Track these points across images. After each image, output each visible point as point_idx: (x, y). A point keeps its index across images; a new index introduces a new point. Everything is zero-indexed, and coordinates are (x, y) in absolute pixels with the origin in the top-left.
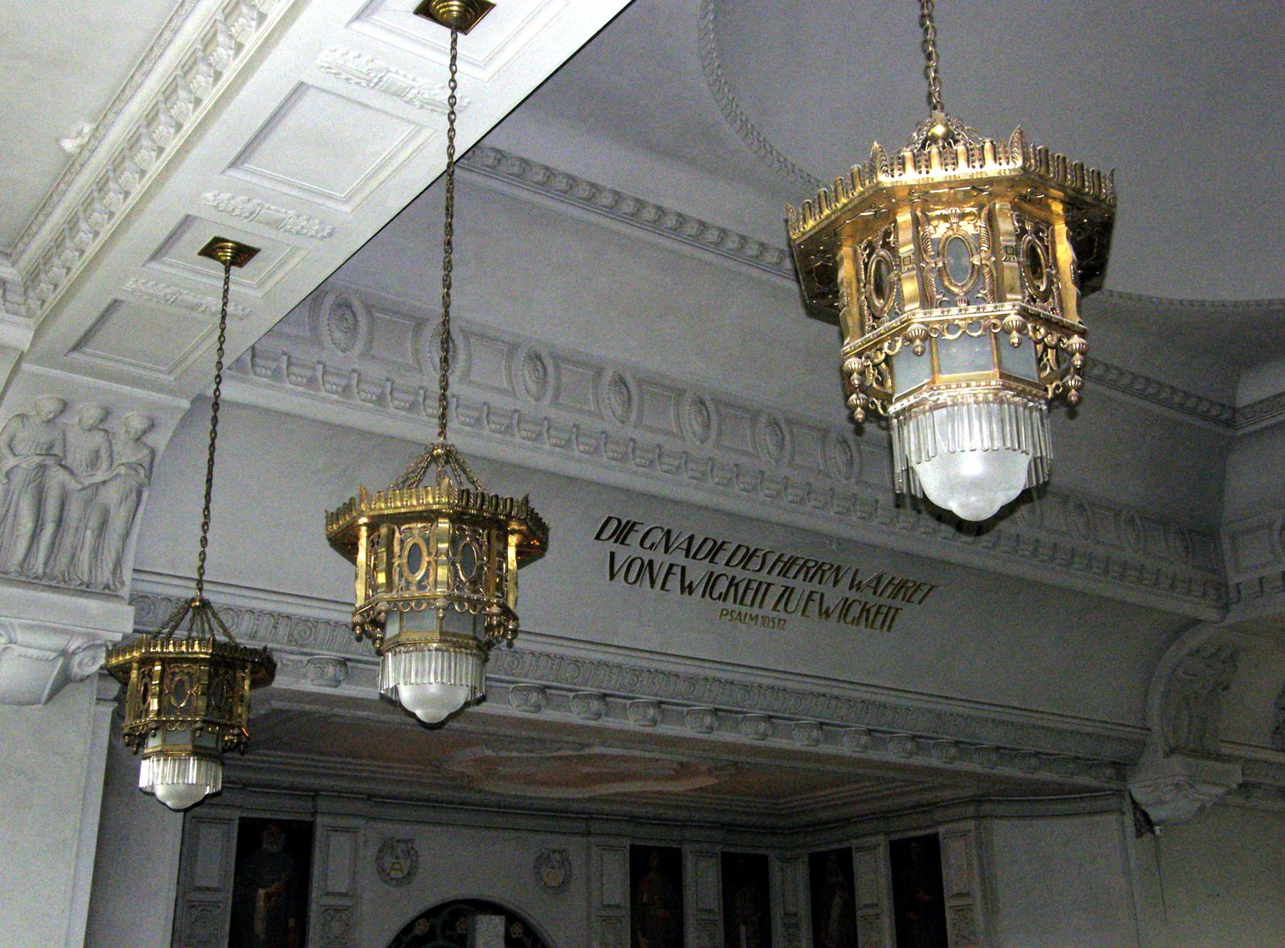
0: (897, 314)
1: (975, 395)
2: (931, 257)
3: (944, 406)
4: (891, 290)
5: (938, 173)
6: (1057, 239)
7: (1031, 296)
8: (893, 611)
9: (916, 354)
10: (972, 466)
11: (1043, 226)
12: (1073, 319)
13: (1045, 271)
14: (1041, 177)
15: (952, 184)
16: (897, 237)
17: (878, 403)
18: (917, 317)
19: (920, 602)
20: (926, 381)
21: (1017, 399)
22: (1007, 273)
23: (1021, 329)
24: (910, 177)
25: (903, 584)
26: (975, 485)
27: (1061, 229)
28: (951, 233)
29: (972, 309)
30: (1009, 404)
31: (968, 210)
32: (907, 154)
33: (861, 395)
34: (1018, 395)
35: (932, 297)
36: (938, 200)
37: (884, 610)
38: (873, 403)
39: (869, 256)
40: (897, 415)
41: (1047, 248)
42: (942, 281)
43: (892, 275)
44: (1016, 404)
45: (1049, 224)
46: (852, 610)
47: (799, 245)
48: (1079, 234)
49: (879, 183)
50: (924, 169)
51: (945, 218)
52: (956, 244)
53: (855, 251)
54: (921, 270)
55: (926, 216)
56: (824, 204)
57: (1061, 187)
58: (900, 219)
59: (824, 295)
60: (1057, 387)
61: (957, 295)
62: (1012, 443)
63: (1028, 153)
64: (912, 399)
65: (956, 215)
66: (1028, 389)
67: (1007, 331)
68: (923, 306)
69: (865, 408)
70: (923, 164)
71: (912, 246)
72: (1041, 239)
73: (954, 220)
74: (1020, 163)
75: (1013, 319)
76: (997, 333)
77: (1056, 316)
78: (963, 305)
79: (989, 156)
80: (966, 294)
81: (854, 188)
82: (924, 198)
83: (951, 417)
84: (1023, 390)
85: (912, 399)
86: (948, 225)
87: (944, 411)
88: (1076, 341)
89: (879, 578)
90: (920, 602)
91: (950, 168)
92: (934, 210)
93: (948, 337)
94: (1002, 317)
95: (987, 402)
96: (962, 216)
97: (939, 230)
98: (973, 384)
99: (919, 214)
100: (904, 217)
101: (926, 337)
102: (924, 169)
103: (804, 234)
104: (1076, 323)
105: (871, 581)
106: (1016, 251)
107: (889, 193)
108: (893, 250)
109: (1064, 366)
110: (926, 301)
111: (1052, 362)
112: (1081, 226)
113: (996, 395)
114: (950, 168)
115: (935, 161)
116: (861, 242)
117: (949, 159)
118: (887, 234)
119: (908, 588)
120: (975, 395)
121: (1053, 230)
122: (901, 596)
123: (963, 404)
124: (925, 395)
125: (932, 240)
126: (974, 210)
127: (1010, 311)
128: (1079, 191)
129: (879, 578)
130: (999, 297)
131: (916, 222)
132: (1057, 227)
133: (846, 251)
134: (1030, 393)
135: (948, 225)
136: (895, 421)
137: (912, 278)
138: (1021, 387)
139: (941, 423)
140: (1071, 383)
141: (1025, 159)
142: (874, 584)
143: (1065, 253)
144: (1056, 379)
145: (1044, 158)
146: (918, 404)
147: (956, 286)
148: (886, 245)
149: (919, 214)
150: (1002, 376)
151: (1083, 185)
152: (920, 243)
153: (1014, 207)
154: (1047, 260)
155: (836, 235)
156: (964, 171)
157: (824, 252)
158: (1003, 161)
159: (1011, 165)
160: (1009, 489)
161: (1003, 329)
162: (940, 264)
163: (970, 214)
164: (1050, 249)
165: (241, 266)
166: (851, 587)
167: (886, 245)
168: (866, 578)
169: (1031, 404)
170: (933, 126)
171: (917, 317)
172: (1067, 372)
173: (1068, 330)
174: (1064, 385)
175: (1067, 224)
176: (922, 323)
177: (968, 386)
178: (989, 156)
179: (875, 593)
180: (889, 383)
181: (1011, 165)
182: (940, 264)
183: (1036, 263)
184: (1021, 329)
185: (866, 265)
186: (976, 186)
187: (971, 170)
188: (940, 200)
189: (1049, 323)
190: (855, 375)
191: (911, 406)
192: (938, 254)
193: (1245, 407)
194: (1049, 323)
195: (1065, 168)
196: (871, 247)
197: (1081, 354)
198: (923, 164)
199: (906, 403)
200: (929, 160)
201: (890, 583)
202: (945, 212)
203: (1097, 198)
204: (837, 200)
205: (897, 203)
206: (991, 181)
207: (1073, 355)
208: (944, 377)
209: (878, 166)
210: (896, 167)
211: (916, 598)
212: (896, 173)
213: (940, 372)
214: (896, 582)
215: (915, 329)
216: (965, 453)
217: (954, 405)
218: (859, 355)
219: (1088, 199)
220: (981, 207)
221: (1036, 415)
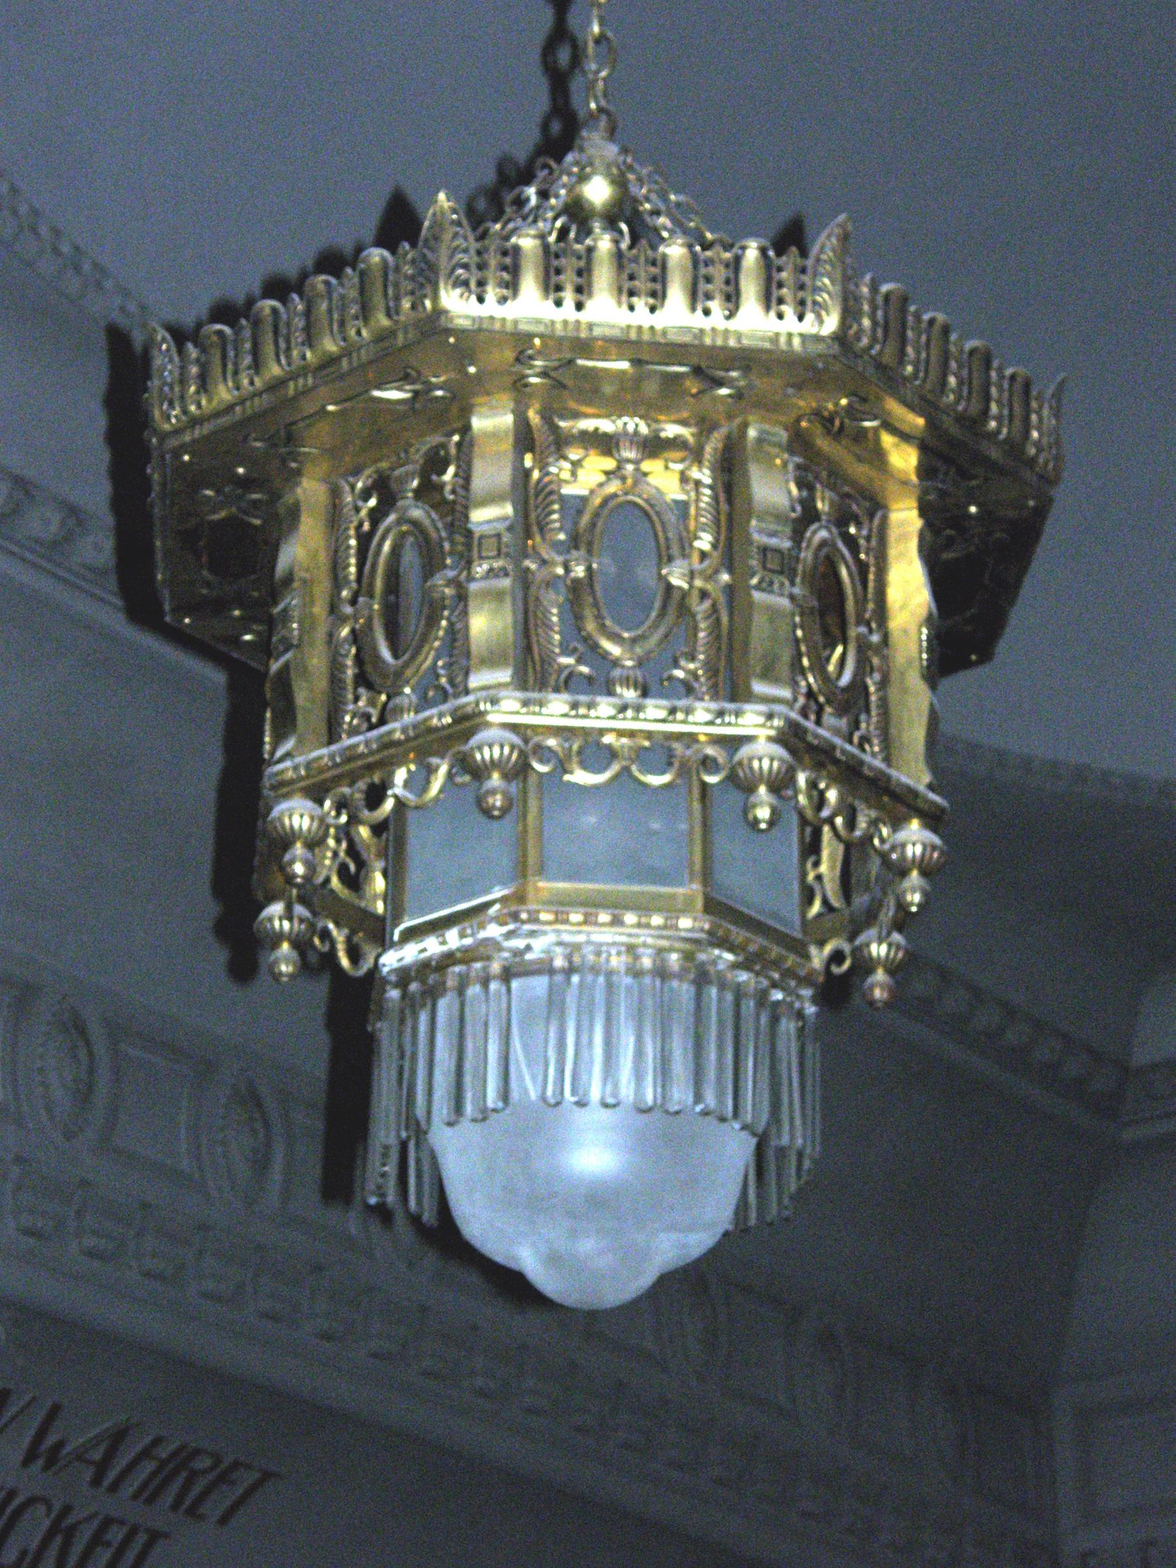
0: (445, 696)
1: (631, 949)
2: (557, 546)
3: (544, 968)
4: (432, 621)
5: (606, 312)
6: (892, 552)
7: (810, 694)
8: (141, 1538)
9: (487, 812)
10: (594, 1153)
11: (863, 506)
12: (914, 774)
13: (854, 631)
14: (880, 366)
15: (644, 350)
16: (465, 476)
17: (339, 936)
18: (505, 709)
19: (223, 1520)
20: (498, 893)
21: (743, 976)
22: (760, 627)
23: (781, 784)
24: (530, 307)
25: (183, 1458)
26: (598, 1202)
27: (905, 519)
28: (613, 487)
29: (655, 709)
30: (722, 986)
31: (671, 430)
32: (527, 243)
33: (299, 910)
34: (745, 965)
35: (547, 660)
36: (591, 391)
37: (116, 1535)
38: (325, 935)
39: (376, 516)
40: (404, 976)
41: (863, 568)
42: (579, 618)
43: (439, 580)
44: (739, 993)
45: (876, 507)
46: (24, 1523)
47: (177, 453)
48: (949, 543)
49: (438, 312)
50: (569, 297)
51: (605, 444)
52: (631, 523)
53: (335, 493)
54: (524, 580)
55: (555, 429)
56: (268, 349)
57: (925, 405)
58: (479, 423)
59: (219, 606)
60: (837, 957)
61: (616, 663)
62: (720, 1096)
63: (857, 299)
64: (453, 939)
65: (636, 440)
66: (776, 951)
67: (742, 783)
68: (521, 682)
69: (300, 945)
70: (568, 279)
71: (508, 509)
72: (851, 542)
73: (629, 454)
74: (831, 323)
75: (765, 754)
76: (710, 785)
77: (873, 759)
78: (630, 694)
79: (750, 290)
80: (640, 663)
81: (365, 313)
82: (564, 376)
83: (555, 1004)
84: (764, 951)
85: (453, 939)
86: (610, 464)
87: (540, 984)
88: (915, 839)
89: (118, 1438)
90: (223, 1520)
91: (640, 303)
92: (576, 415)
93: (580, 777)
94: (733, 743)
95: (662, 972)
96: (654, 446)
97: (585, 477)
98: (630, 918)
99: (533, 416)
100: (492, 421)
101: (519, 771)
102: (569, 297)
103: (195, 422)
104: (921, 788)
105: (97, 1440)
106: (786, 565)
107: (469, 343)
108: (454, 513)
109: (861, 900)
110: (533, 672)
111: (831, 887)
112: (959, 521)
113: (688, 957)
114: (640, 303)
115: (603, 276)
116: (357, 472)
117: (642, 279)
118: (436, 462)
119: (193, 1475)
120: (631, 949)
121: (885, 520)
122: (169, 1498)
123: (595, 970)
124: (493, 931)
125: (563, 499)
126: (686, 432)
127: (756, 727)
128: (974, 423)
129: (118, 1438)
130: (732, 689)
131: (524, 439)
132: (895, 517)
133: (310, 490)
134: (776, 964)
135: (610, 464)
136: (394, 994)
137: (499, 596)
138: (757, 942)
139: (528, 1016)
140: (878, 950)
141: (849, 314)
142: (97, 1455)
143: (908, 589)
144: (834, 933)
145: (895, 319)
146: (466, 956)
147: (615, 638)
148: (428, 491)
149: (533, 416)
150: (712, 906)
151: (985, 411)
152: (531, 499)
153: (799, 442)
154: (861, 602)
155: (290, 439)
156: (675, 316)
157: (246, 484)
158: (788, 310)
159: (809, 325)
160: (691, 1228)
161: (732, 779)
162: (579, 571)
163: (676, 443)
164: (872, 574)
165: (590, 295)
166: (30, 1458)
167: (428, 491)
168: (79, 1434)
169: (778, 996)
170: (583, 178)
171: (505, 709)
172: (870, 917)
173: (898, 804)
174: (857, 952)
175: (923, 511)
176: (514, 728)
177: (617, 921)
178: (750, 290)
179: (96, 1482)
180: (379, 883)
181: (809, 325)
182: (579, 571)
183: (837, 604)
184: (781, 784)
185: (365, 540)
186: (708, 363)
187: (697, 320)
188: (596, 391)
189: (851, 775)
190: (299, 849)
191: (449, 959)
192: (575, 541)
193: (1154, 1067)
194: (851, 775)
195: (946, 357)
196: (386, 492)
197: (924, 873)
198: (568, 279)
199: (432, 946)
200: (585, 272)
201: (146, 1454)
202: (607, 426)
203: (1015, 447)
204: (310, 341)
205: (478, 377)
206: (747, 359)
207: (903, 873)
208: (545, 886)
209: (444, 264)
210: (492, 274)
211: (214, 1507)
212: (491, 293)
213: (541, 871)
214: (163, 1452)
215: (490, 746)
216: (586, 1116)
217: (570, 970)
218: (316, 794)
219: (994, 454)
220: (705, 426)
221: (788, 1026)
